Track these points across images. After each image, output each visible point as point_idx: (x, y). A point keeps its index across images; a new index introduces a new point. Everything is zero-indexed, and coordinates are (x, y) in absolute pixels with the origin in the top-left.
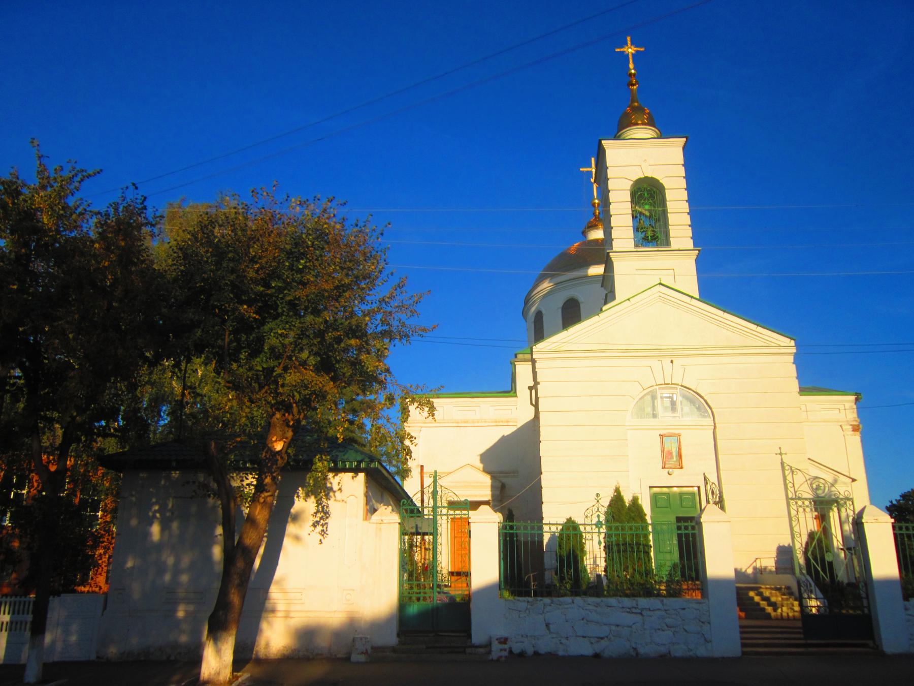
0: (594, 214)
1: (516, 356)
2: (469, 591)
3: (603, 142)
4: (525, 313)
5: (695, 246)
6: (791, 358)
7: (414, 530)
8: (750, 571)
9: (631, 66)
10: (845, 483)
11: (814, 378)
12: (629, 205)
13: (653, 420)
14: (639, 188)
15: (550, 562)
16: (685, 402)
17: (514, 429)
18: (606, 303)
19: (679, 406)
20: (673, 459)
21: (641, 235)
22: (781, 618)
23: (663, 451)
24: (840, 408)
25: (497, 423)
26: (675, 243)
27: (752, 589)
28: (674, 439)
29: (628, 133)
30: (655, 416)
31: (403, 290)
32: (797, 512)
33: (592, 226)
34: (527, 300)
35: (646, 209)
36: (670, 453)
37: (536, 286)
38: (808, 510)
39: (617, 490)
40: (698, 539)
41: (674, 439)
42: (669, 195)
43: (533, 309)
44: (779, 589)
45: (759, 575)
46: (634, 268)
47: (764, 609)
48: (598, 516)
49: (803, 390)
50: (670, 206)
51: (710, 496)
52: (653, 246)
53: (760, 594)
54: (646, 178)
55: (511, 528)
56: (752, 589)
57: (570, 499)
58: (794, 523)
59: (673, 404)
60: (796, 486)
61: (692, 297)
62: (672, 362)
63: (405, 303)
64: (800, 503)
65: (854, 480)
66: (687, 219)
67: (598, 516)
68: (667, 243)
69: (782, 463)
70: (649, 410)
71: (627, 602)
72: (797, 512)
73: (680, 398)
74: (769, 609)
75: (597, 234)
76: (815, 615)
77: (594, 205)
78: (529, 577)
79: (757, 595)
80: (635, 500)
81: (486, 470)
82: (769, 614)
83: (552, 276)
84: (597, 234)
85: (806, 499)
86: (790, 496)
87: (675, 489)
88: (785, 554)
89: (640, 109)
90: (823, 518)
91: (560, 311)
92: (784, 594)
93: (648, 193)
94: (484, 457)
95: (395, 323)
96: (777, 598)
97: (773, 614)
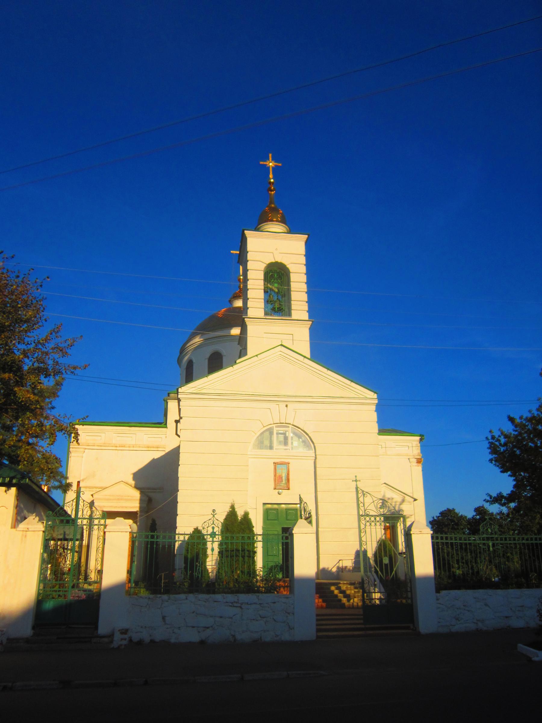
0: (239, 287)
1: (169, 396)
2: (100, 589)
3: (246, 232)
4: (179, 361)
5: (309, 318)
6: (374, 408)
7: (61, 537)
8: (334, 570)
9: (271, 176)
10: (409, 502)
11: (390, 423)
12: (262, 282)
13: (269, 451)
14: (271, 271)
15: (179, 563)
16: (296, 438)
17: (163, 453)
18: (240, 357)
19: (290, 441)
20: (282, 482)
21: (270, 306)
22: (352, 607)
23: (275, 476)
24: (408, 446)
25: (149, 448)
26: (295, 315)
27: (334, 584)
28: (278, 466)
29: (265, 227)
30: (271, 448)
31: (59, 334)
32: (365, 525)
33: (236, 297)
34: (182, 350)
35: (275, 287)
36: (280, 477)
37: (190, 339)
38: (378, 524)
39: (233, 507)
40: (290, 547)
41: (284, 467)
42: (293, 277)
43: (186, 358)
44: (351, 584)
45: (340, 573)
46: (262, 331)
47: (340, 600)
48: (213, 528)
49: (383, 430)
50: (293, 286)
51: (303, 513)
52: (279, 316)
53: (339, 588)
54: (277, 263)
55: (152, 537)
56: (334, 584)
57: (196, 513)
58: (362, 534)
59: (286, 438)
60: (366, 507)
61: (305, 357)
62: (287, 406)
63: (60, 345)
64: (368, 519)
65: (415, 500)
66: (305, 297)
67: (213, 528)
68: (290, 315)
69: (357, 488)
70: (267, 443)
71: (230, 598)
72: (365, 525)
73: (292, 435)
74: (344, 600)
75: (239, 303)
76: (378, 604)
77: (239, 280)
78: (161, 577)
79: (337, 589)
80: (246, 515)
81: (136, 487)
82: (344, 604)
83: (203, 334)
84: (239, 303)
85: (372, 516)
86: (361, 513)
87: (283, 506)
88: (360, 555)
89: (275, 210)
90: (391, 529)
91: (207, 361)
92: (355, 588)
93: (277, 274)
94: (137, 476)
95: (50, 362)
96: (351, 591)
97: (347, 604)
